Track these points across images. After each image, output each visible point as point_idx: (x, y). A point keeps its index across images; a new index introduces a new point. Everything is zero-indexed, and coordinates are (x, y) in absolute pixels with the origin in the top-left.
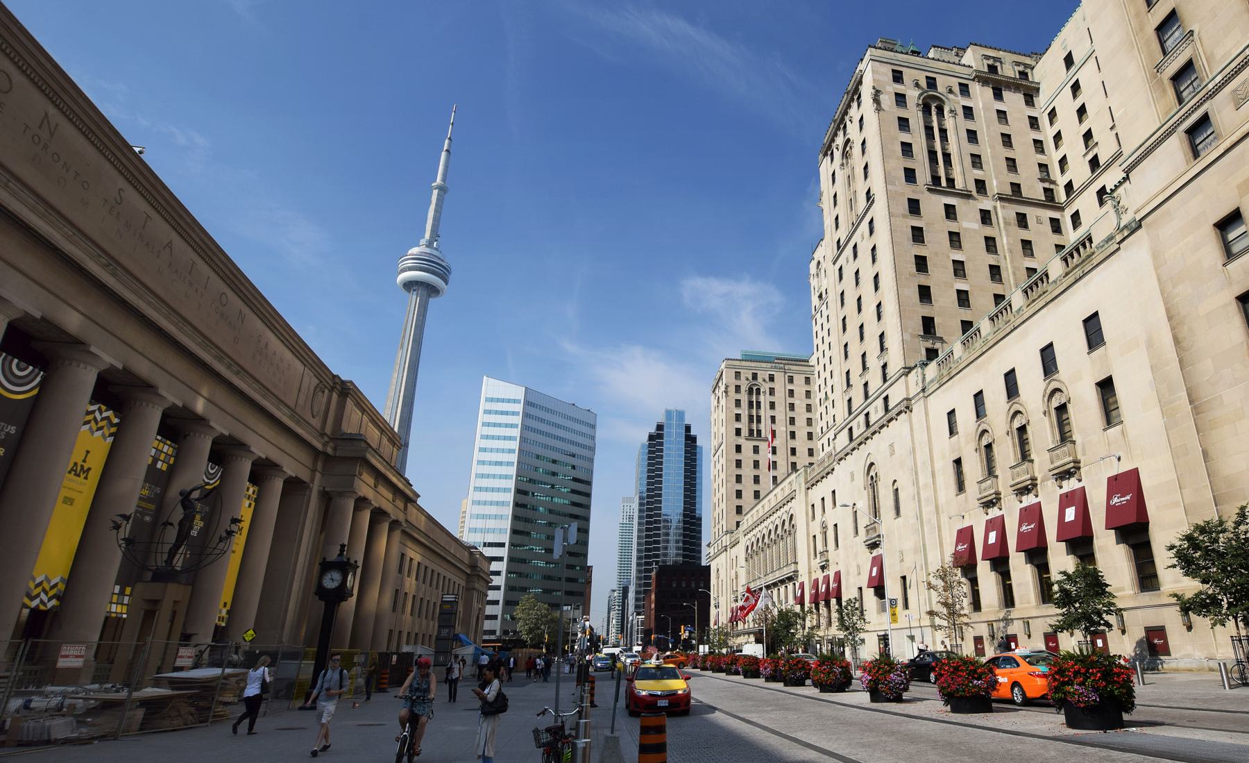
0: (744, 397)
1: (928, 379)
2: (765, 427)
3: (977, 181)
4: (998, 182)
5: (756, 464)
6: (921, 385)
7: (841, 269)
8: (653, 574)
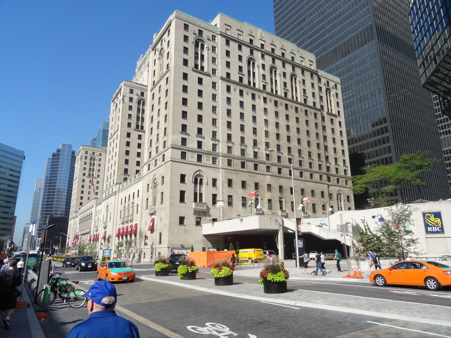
0: (88, 161)
3: (213, 69)
8: (47, 221)
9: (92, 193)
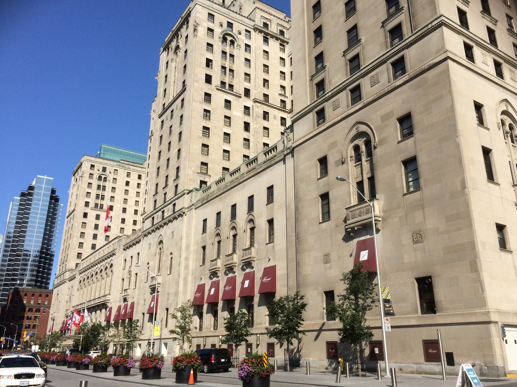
4: (257, 92)
5: (96, 227)
7: (163, 122)
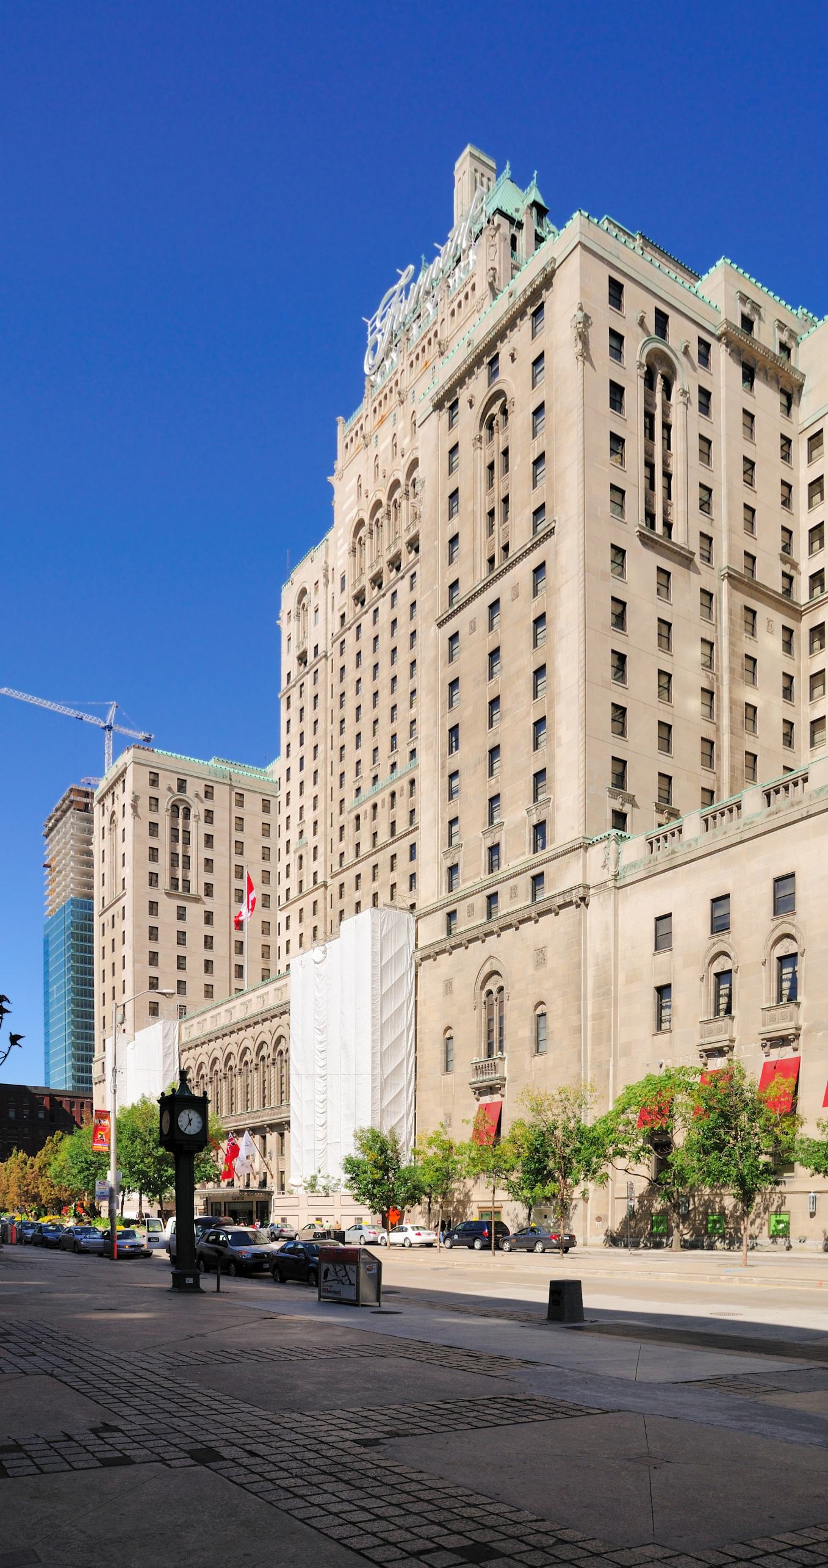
1: (624, 861)
2: (197, 878)
6: (612, 869)
9: (257, 880)
